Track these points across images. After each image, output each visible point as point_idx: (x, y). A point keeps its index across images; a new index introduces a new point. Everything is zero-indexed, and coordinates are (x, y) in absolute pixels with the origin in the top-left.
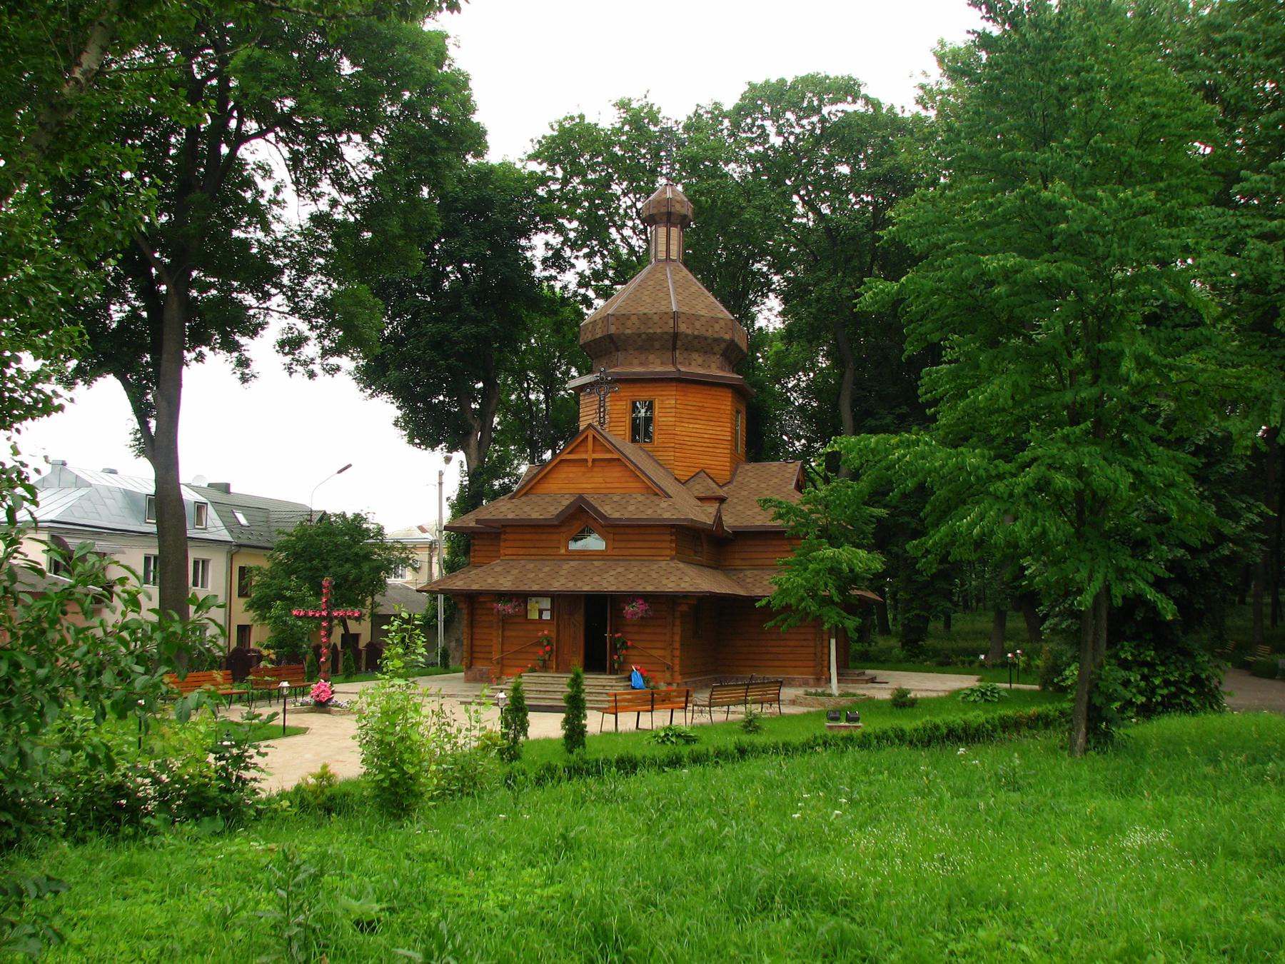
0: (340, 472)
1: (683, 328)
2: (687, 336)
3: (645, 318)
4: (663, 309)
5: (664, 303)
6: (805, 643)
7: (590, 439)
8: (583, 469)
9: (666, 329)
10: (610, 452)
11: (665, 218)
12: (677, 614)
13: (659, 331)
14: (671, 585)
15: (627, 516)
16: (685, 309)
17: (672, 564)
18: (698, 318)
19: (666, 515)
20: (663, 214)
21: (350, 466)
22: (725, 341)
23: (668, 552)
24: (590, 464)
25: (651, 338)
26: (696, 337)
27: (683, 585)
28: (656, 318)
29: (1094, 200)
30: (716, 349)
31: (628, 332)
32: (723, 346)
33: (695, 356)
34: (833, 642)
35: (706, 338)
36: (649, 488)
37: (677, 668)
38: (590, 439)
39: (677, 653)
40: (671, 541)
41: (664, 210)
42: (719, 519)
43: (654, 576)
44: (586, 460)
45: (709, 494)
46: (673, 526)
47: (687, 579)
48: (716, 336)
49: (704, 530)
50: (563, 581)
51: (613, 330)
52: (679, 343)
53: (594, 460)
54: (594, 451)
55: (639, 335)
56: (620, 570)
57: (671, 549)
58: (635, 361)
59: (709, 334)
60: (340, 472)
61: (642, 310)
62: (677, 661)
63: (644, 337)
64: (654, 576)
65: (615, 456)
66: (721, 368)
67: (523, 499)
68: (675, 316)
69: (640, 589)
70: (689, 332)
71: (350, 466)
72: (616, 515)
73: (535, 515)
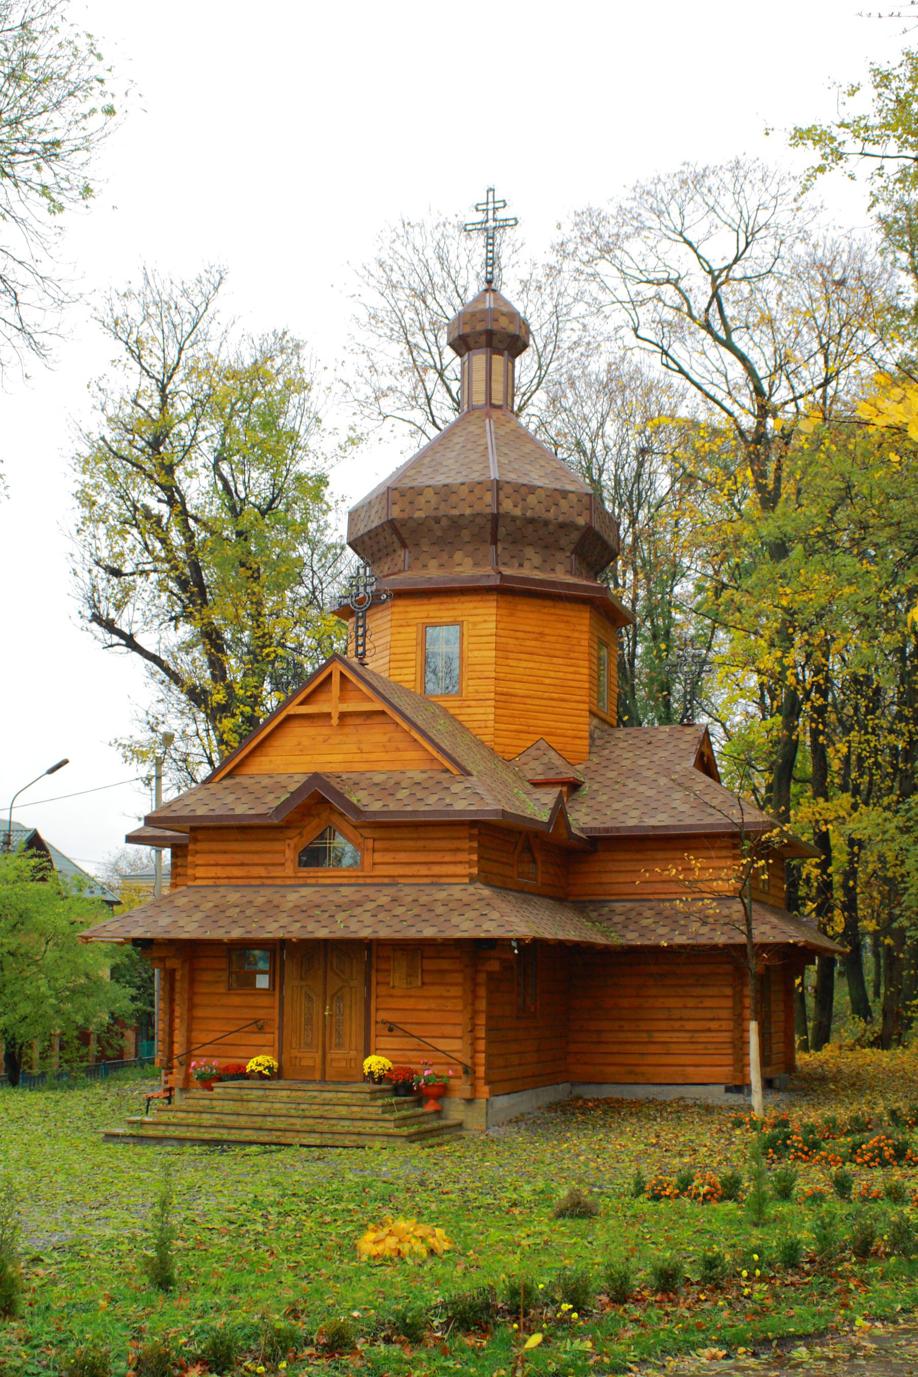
0: (52, 771)
1: (507, 505)
2: (514, 519)
3: (446, 491)
4: (476, 477)
5: (477, 467)
6: (714, 1025)
7: (336, 679)
8: (325, 731)
9: (478, 508)
10: (369, 699)
11: (483, 339)
12: (482, 977)
13: (468, 512)
14: (466, 925)
15: (392, 807)
16: (512, 477)
17: (471, 889)
18: (532, 489)
19: (460, 805)
20: (480, 334)
21: (65, 762)
22: (577, 527)
23: (461, 870)
24: (335, 721)
25: (456, 523)
26: (531, 521)
27: (486, 926)
28: (464, 491)
29: (823, 1079)
30: (563, 542)
31: (419, 515)
32: (575, 536)
33: (529, 552)
34: (753, 1026)
35: (546, 523)
36: (434, 759)
37: (481, 1071)
38: (336, 679)
39: (481, 1045)
40: (471, 851)
41: (480, 327)
42: (559, 813)
43: (440, 910)
44: (328, 715)
45: (551, 775)
46: (473, 824)
47: (495, 915)
48: (561, 519)
49: (537, 834)
50: (284, 920)
51: (396, 513)
52: (502, 531)
53: (343, 716)
54: (342, 699)
55: (437, 520)
56: (384, 900)
57: (470, 863)
58: (433, 563)
59: (551, 515)
60: (52, 771)
61: (440, 479)
62: (481, 1058)
63: (444, 522)
64: (440, 910)
65: (378, 706)
66: (569, 572)
67: (226, 783)
68: (498, 486)
69: (412, 934)
70: (517, 512)
71: (65, 762)
72: (376, 806)
73: (240, 810)
